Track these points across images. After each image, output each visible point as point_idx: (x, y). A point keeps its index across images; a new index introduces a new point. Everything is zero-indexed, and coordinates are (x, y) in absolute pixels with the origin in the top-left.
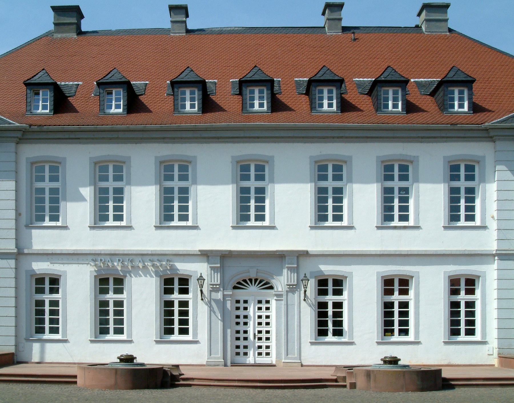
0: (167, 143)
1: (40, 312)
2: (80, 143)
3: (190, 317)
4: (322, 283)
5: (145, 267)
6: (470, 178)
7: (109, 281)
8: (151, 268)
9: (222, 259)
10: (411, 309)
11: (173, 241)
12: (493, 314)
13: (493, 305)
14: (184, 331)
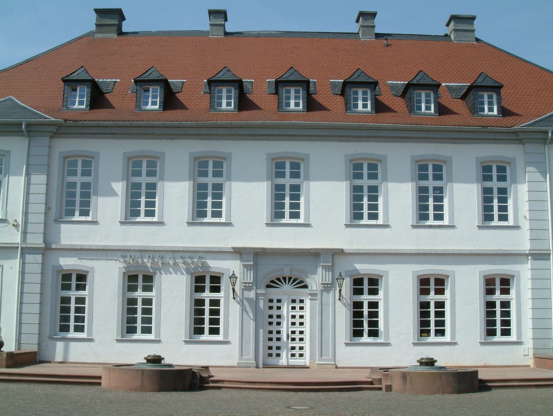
2: (114, 138)
3: (222, 317)
5: (175, 264)
6: (218, 174)
7: (138, 279)
8: (181, 265)
9: (255, 257)
11: (206, 237)
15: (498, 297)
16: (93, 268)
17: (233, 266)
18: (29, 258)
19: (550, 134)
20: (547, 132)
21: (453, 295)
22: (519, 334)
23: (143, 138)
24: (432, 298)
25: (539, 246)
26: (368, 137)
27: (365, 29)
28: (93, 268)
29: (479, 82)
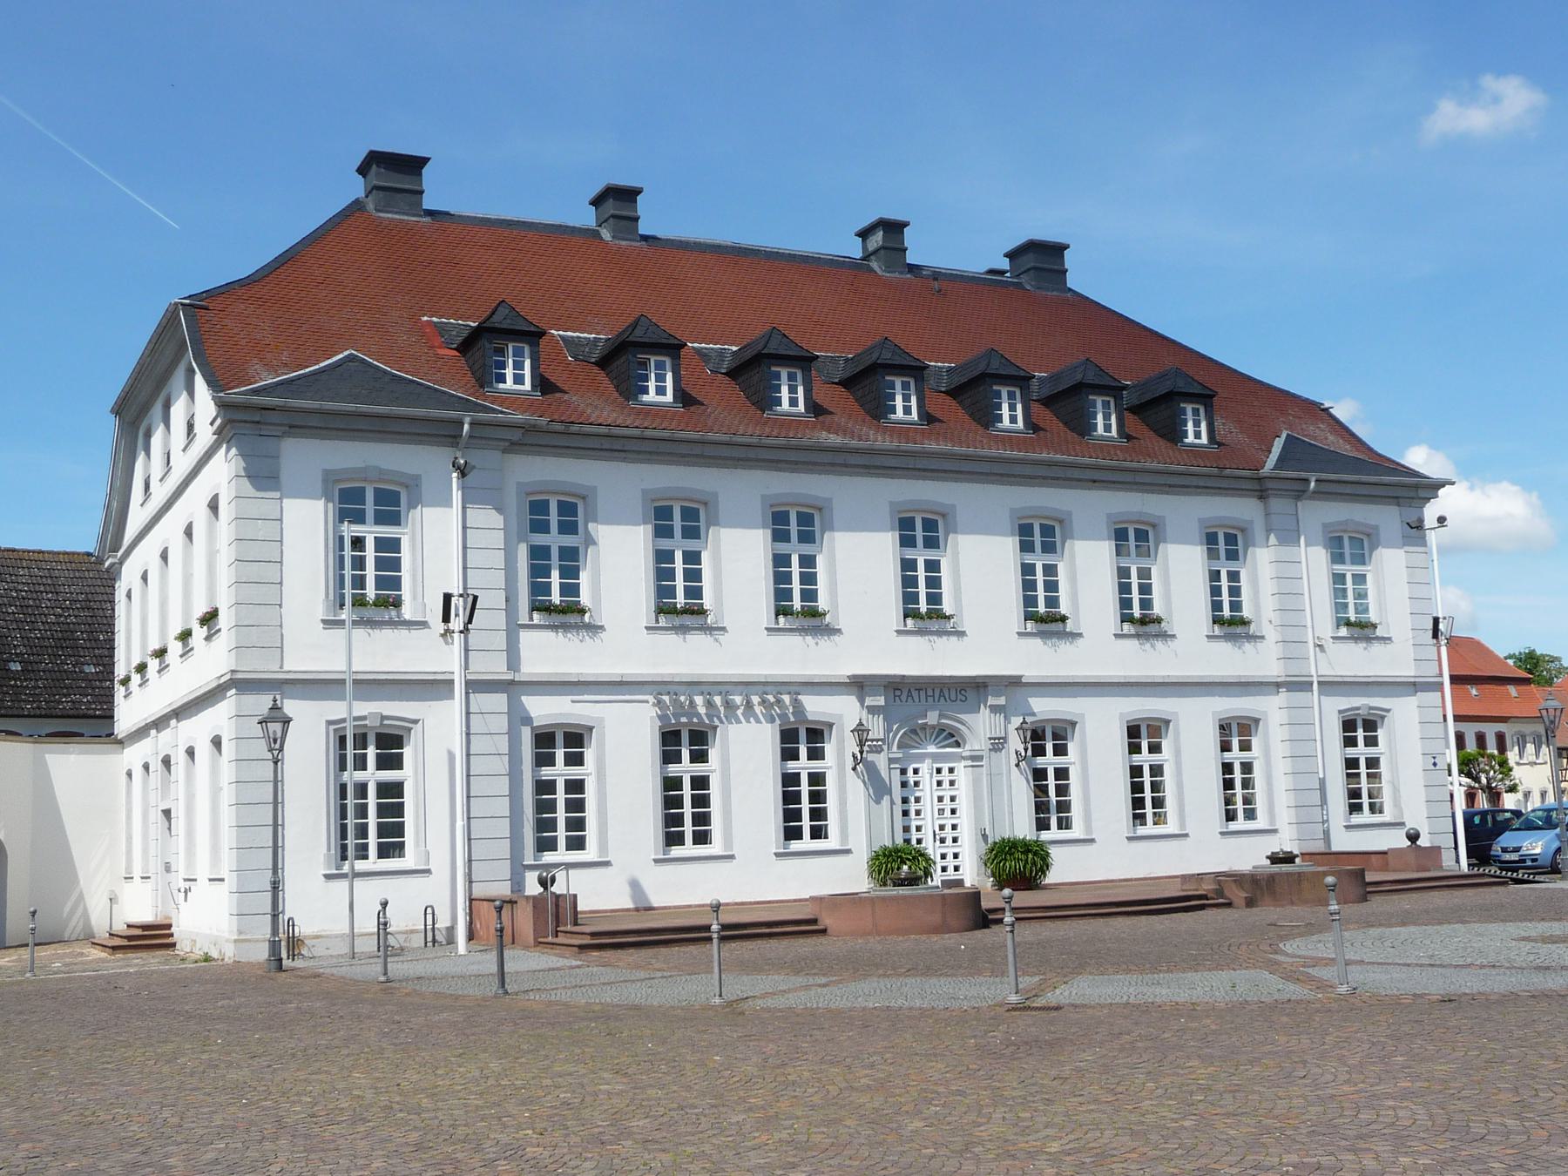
0: (780, 470)
1: (545, 808)
2: (624, 460)
3: (409, 819)
4: (544, 739)
5: (749, 705)
6: (568, 528)
7: (683, 739)
8: (758, 709)
9: (900, 692)
10: (590, 795)
11: (795, 657)
12: (1282, 783)
13: (1281, 767)
14: (702, 838)
15: (1049, 761)
16: (601, 720)
17: (844, 711)
18: (481, 701)
19: (1313, 484)
20: (1307, 481)
21: (725, 761)
22: (1272, 815)
23: (649, 461)
24: (685, 768)
25: (1295, 669)
26: (1044, 478)
27: (381, 194)
28: (601, 720)
29: (638, 335)
